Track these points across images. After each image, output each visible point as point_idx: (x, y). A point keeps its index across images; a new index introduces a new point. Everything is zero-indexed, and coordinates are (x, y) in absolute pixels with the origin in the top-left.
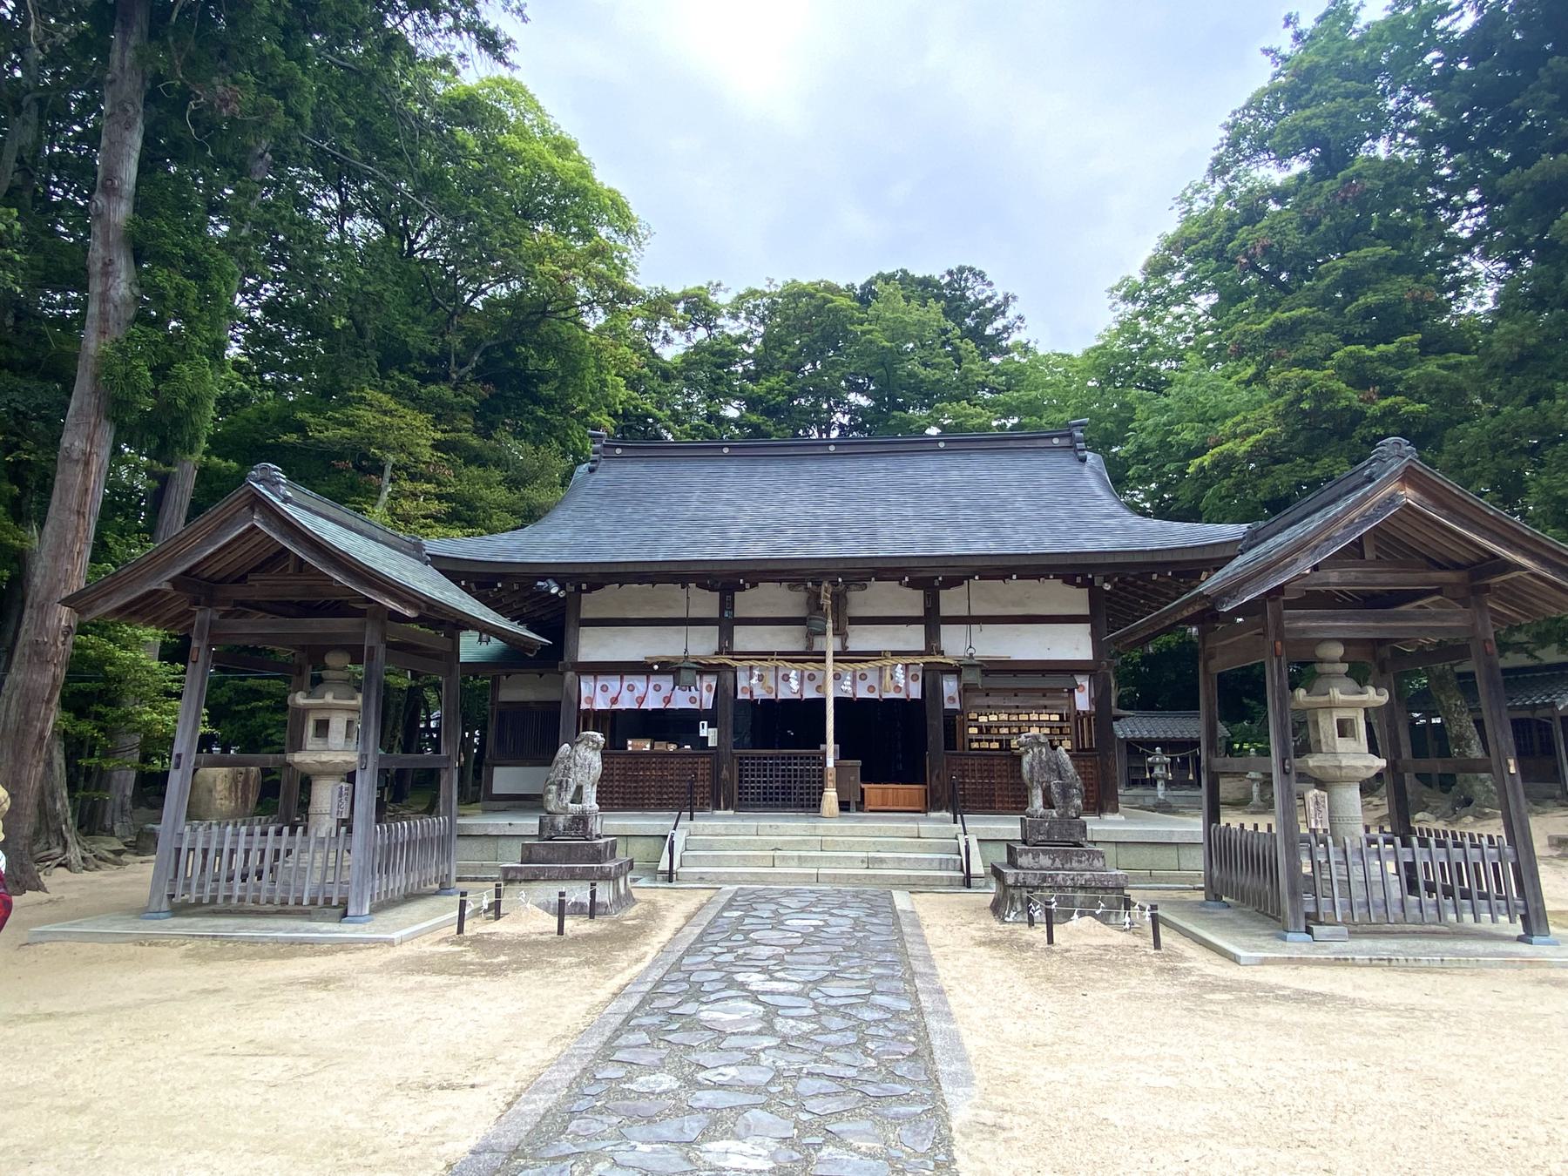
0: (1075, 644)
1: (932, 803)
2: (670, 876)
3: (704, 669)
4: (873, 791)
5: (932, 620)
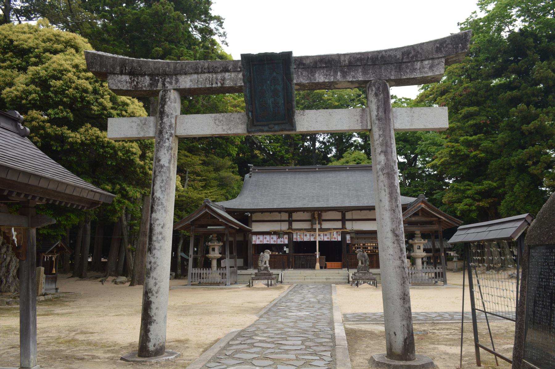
1: (343, 267)
2: (281, 282)
3: (286, 233)
4: (328, 264)
5: (344, 220)
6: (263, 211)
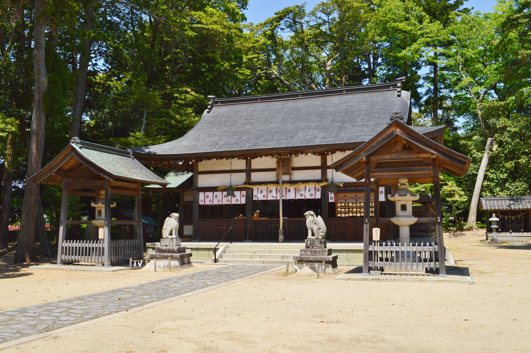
6: (208, 156)
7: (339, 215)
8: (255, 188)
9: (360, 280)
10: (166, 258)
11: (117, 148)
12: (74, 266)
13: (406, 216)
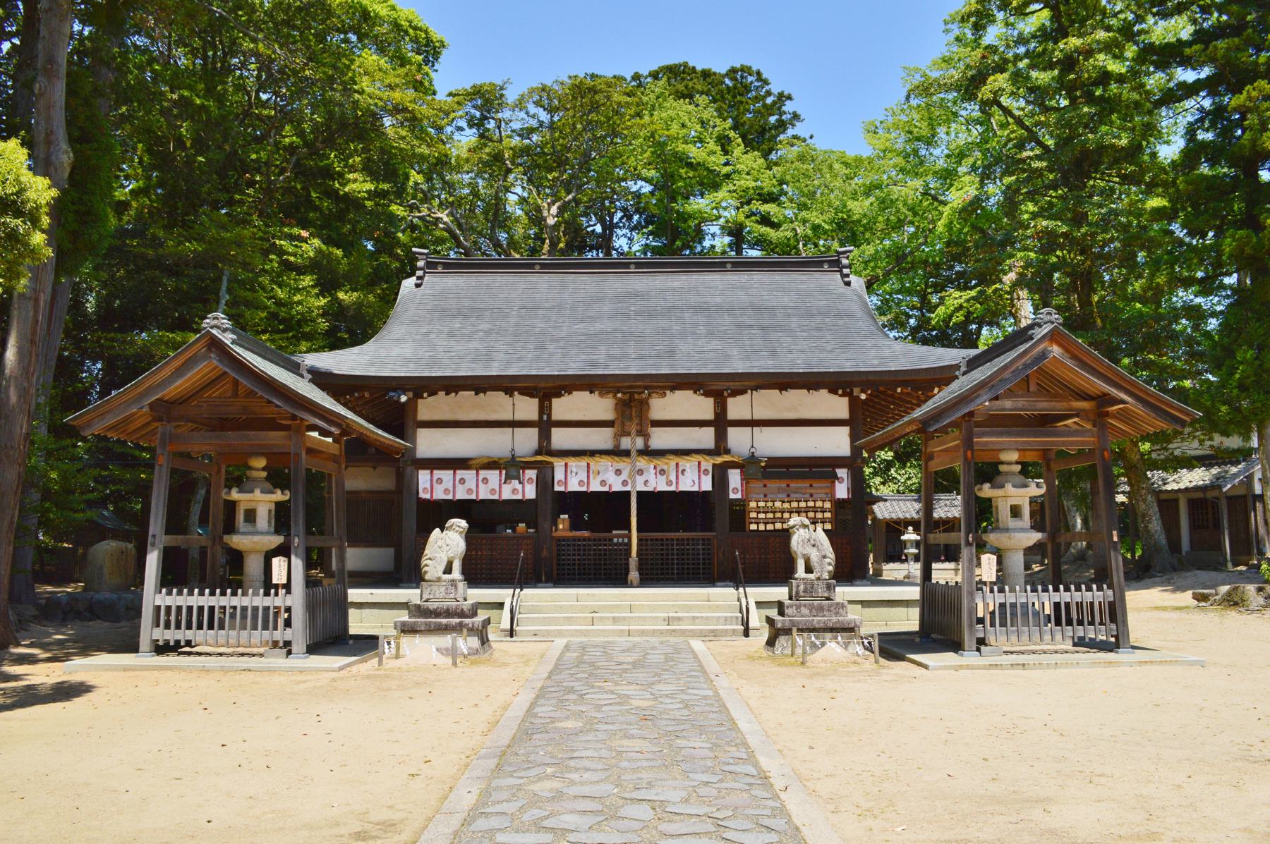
0: (837, 442)
6: (452, 385)
7: (753, 527)
8: (559, 465)
9: (984, 667)
10: (446, 629)
11: (172, 355)
12: (181, 658)
13: (1023, 530)
